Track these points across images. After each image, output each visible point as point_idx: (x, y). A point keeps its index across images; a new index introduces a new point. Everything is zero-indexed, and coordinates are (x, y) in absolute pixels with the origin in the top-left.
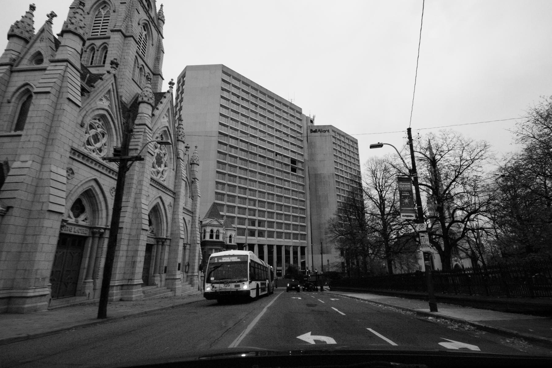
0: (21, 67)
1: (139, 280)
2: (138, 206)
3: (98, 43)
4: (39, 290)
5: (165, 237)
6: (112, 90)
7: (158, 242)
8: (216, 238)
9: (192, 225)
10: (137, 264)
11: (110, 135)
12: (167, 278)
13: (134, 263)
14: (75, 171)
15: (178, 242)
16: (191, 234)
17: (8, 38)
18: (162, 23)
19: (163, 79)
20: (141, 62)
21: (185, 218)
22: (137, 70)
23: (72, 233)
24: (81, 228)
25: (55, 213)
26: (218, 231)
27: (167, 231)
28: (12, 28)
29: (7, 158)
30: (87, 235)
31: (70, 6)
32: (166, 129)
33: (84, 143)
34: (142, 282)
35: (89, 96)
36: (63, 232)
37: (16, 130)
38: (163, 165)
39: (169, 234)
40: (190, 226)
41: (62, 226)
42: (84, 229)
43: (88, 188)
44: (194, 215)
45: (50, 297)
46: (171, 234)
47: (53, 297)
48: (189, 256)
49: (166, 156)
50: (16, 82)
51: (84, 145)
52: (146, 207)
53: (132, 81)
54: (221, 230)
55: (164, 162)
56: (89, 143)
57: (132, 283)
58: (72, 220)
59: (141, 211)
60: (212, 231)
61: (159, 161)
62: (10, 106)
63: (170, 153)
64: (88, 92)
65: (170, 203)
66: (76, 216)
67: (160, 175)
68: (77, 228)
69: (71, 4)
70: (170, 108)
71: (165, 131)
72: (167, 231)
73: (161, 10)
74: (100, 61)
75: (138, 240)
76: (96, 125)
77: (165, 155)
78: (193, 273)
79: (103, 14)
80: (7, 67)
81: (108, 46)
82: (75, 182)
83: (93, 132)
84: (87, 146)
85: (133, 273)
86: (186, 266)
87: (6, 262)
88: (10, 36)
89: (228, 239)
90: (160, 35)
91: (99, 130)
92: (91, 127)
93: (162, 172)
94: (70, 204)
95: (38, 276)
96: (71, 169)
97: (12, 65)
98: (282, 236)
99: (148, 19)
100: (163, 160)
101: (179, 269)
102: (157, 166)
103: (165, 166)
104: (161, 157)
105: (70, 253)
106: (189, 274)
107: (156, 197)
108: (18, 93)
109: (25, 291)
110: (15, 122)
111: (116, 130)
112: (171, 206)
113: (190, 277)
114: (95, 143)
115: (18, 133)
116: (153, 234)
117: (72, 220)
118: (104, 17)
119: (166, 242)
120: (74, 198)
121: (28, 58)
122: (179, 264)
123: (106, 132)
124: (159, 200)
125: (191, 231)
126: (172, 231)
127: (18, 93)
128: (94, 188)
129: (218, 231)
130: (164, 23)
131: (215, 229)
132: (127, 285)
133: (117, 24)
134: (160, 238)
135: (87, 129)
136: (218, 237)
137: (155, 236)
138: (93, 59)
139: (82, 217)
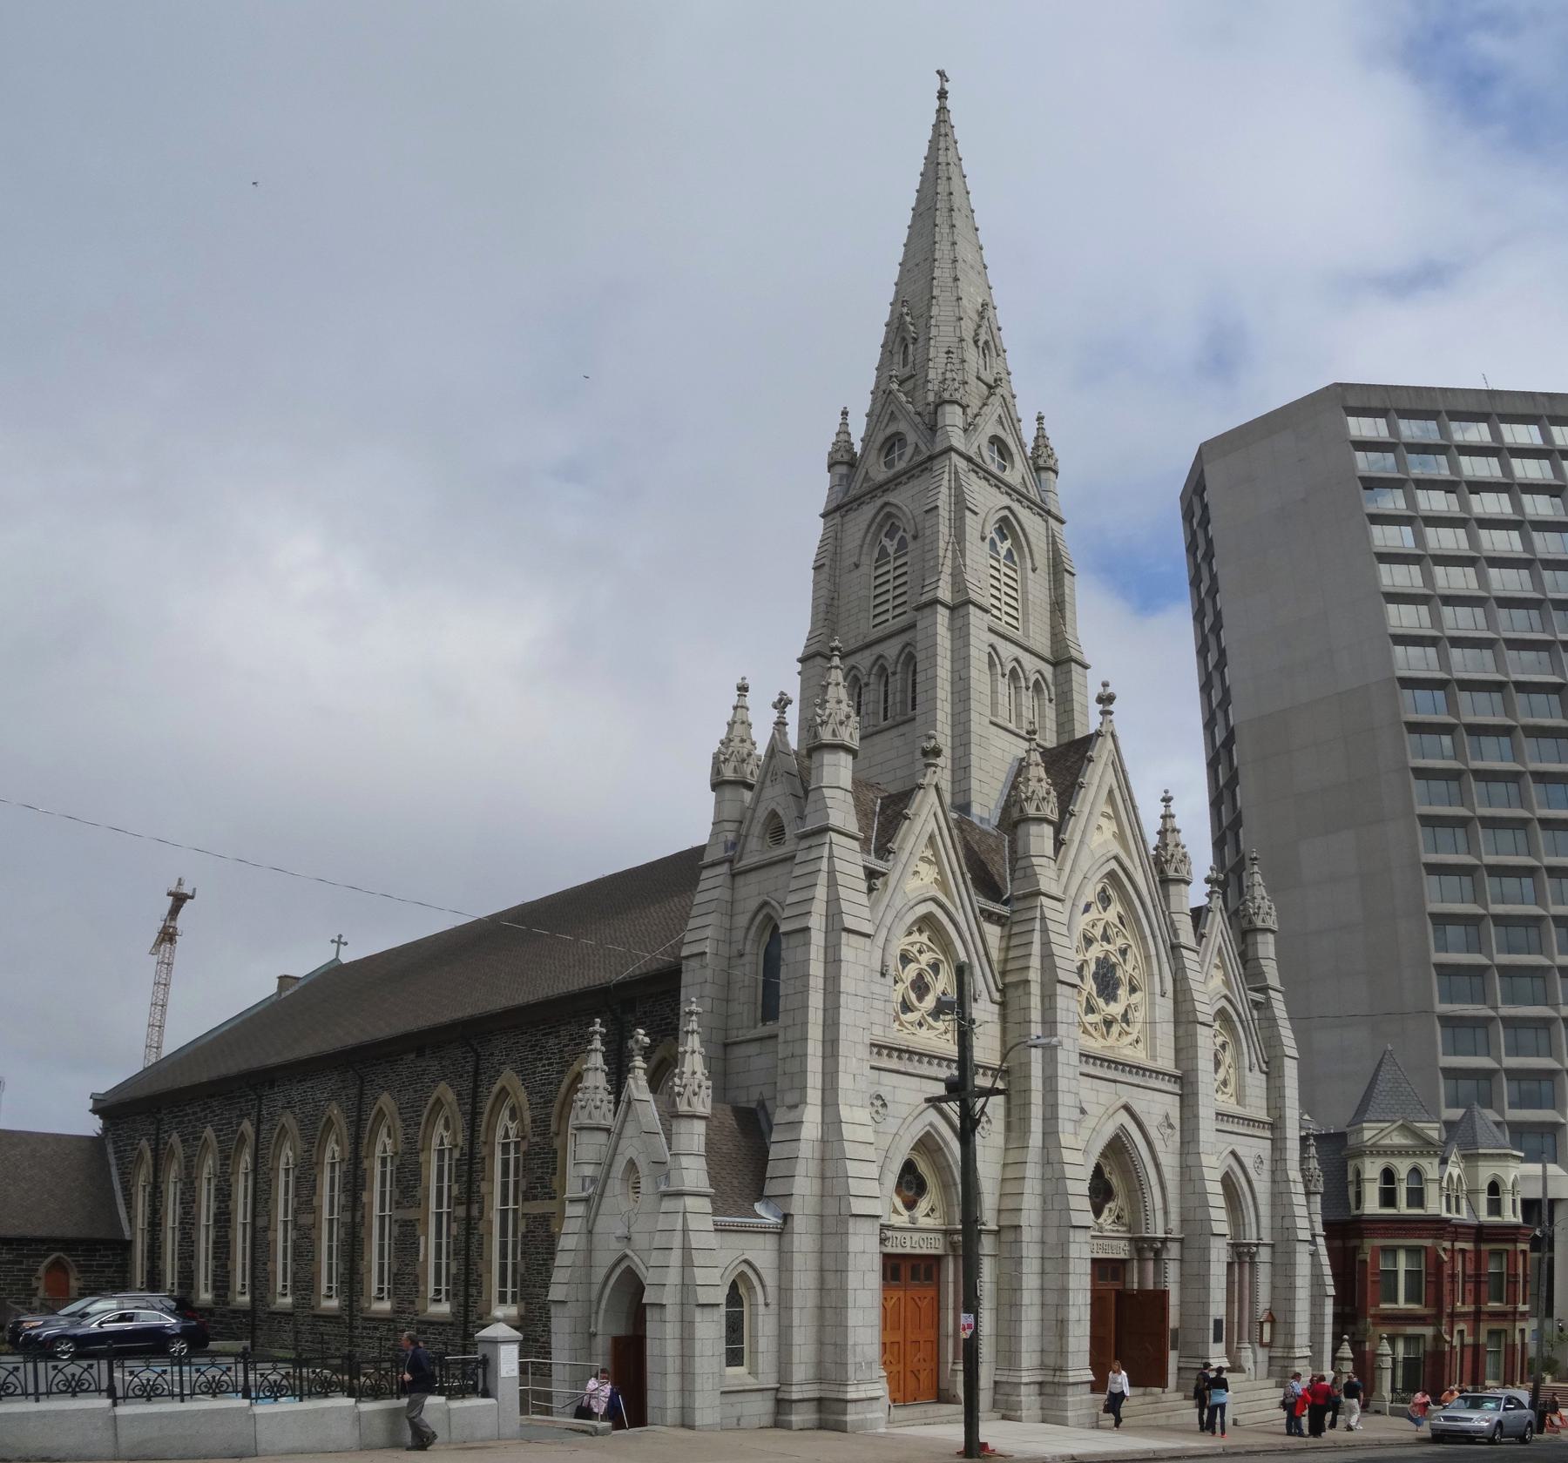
0: (748, 861)
1: (1082, 1372)
2: (1054, 1158)
3: (891, 649)
4: (865, 1386)
5: (1160, 1234)
6: (937, 832)
7: (1140, 1251)
8: (1409, 1205)
9: (1273, 1172)
10: (1071, 1327)
11: (1237, 1041)
12: (1182, 1365)
13: (1062, 1325)
14: (888, 1098)
15: (1206, 1249)
16: (1273, 1205)
17: (713, 790)
18: (1052, 475)
19: (1086, 667)
20: (1007, 651)
21: (1240, 1153)
22: (1003, 685)
23: (908, 1250)
24: (924, 1235)
25: (863, 1219)
26: (1416, 1172)
27: (1166, 1213)
28: (718, 762)
29: (761, 1093)
30: (940, 1252)
31: (812, 564)
32: (1113, 865)
33: (897, 1013)
34: (1092, 1378)
35: (886, 884)
36: (889, 1250)
37: (765, 1019)
38: (1122, 992)
39: (1174, 1223)
40: (1266, 1176)
41: (883, 1241)
42: (932, 1235)
43: (923, 1133)
44: (1278, 1135)
45: (886, 1401)
46: (1184, 1221)
47: (894, 1401)
48: (1274, 1288)
49: (1129, 956)
50: (745, 899)
51: (897, 1018)
52: (1076, 1157)
53: (991, 726)
54: (1431, 1168)
55: (1125, 980)
56: (906, 1007)
57: (1063, 1380)
58: (902, 1219)
59: (1063, 1171)
60: (1388, 1175)
61: (1107, 982)
62: (744, 965)
63: (1144, 938)
64: (884, 874)
65: (1167, 1117)
66: (910, 1205)
67: (1115, 1029)
68: (916, 1236)
69: (814, 557)
70: (1115, 786)
71: (1111, 875)
72: (1166, 1213)
73: (1041, 437)
74: (903, 702)
75: (1065, 1259)
76: (915, 949)
77: (1123, 952)
78: (1291, 1347)
79: (891, 550)
80: (725, 868)
81: (914, 652)
82: (891, 1125)
83: (911, 971)
84: (903, 1017)
85: (1063, 1352)
86: (1261, 1324)
87: (803, 1328)
88: (717, 785)
89: (1483, 1199)
90: (1051, 520)
91: (926, 958)
92: (905, 959)
93: (1125, 1015)
94: (892, 1179)
95: (857, 1360)
96: (879, 1097)
97: (731, 861)
98: (1419, 1301)
99: (1006, 501)
100: (1119, 973)
101: (1217, 1339)
102: (1101, 1002)
103: (1133, 990)
104: (1114, 966)
105: (913, 1299)
106: (1278, 1353)
107: (1111, 1111)
108: (754, 929)
109: (842, 1388)
110: (760, 1002)
111: (1243, 1027)
112: (1171, 1126)
113: (1282, 1363)
114: (920, 998)
115: (770, 1028)
116: (1123, 1225)
117: (902, 1219)
118: (895, 559)
119: (1168, 1250)
120: (896, 1167)
121: (756, 834)
122: (1218, 1323)
123: (942, 957)
124: (1123, 1117)
125: (1273, 1195)
126: (1183, 1210)
127: (754, 929)
128: (1232, 1170)
129: (1416, 1172)
130: (1056, 473)
131: (1402, 1167)
132: (1053, 1383)
133: (927, 582)
134: (1144, 1239)
135: (897, 970)
136: (1416, 1197)
137: (1129, 1231)
138: (886, 701)
139: (923, 1205)
